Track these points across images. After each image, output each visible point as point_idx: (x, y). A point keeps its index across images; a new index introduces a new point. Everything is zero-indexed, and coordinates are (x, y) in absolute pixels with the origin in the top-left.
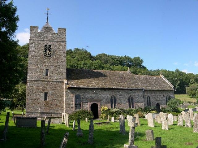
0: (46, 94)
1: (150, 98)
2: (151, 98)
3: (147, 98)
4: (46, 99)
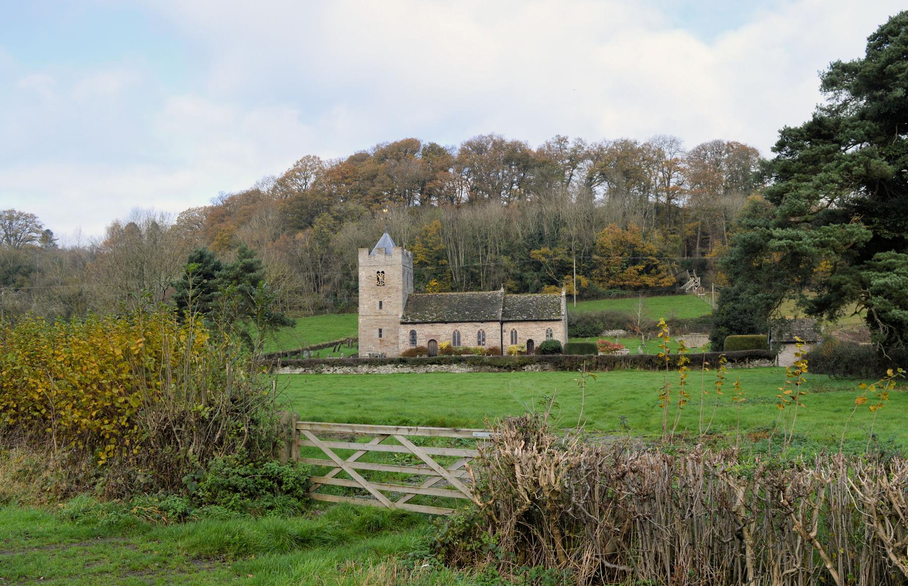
0: (380, 331)
1: (516, 332)
2: (518, 331)
3: (512, 332)
4: (380, 336)
